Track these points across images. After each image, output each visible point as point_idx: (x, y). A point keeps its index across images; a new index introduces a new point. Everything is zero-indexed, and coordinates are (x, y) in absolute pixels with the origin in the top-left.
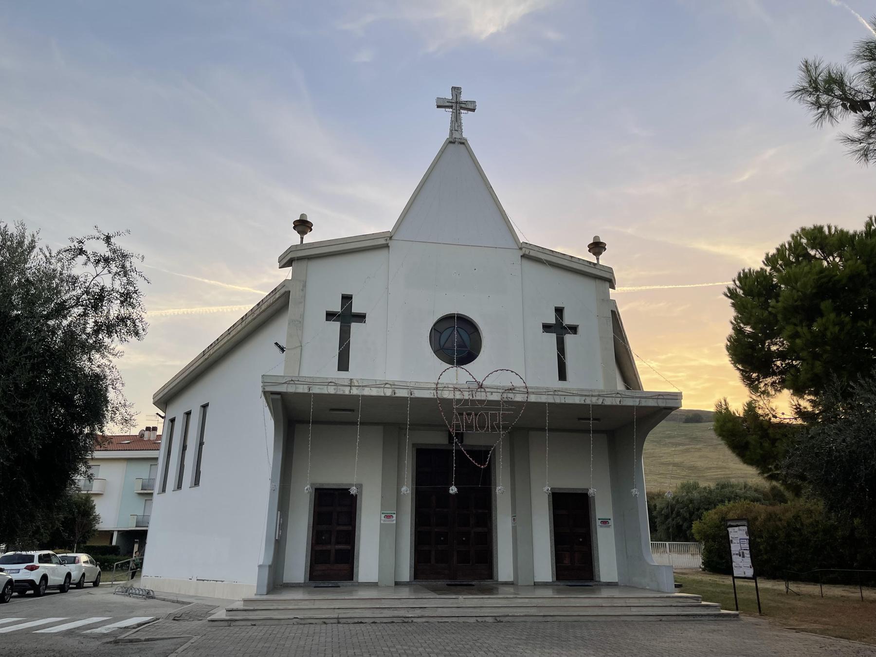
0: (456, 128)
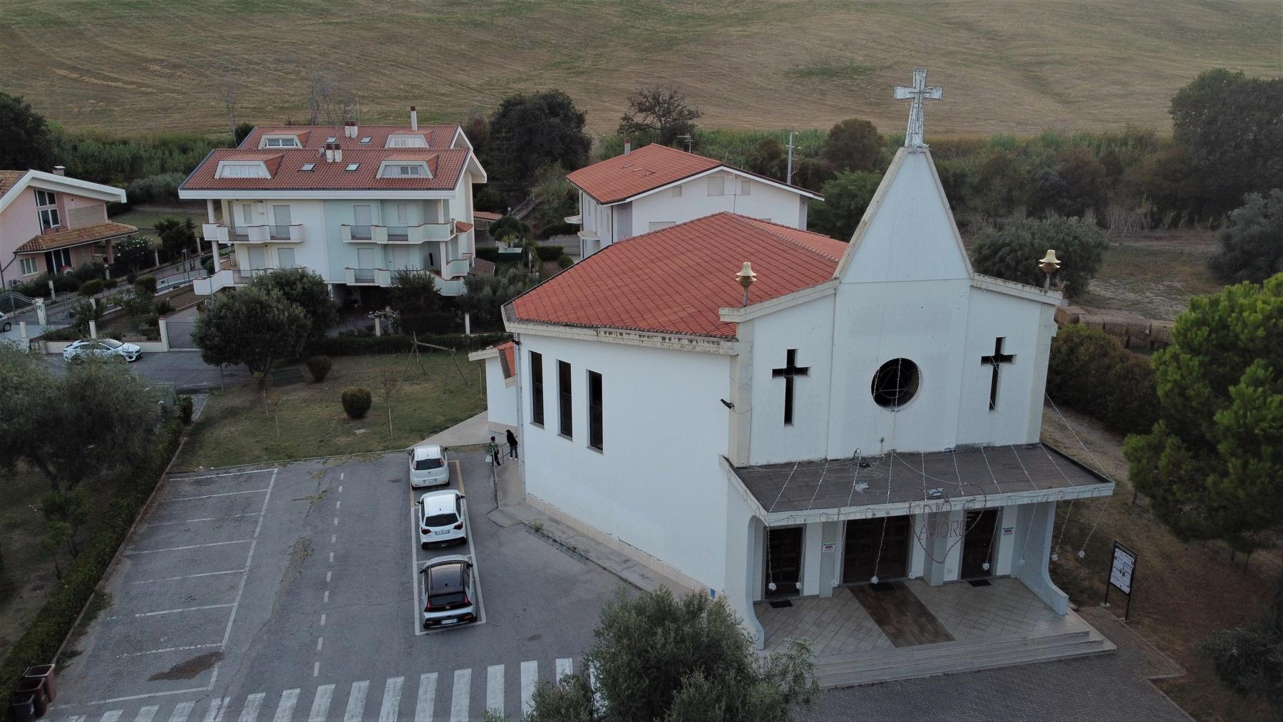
0: (917, 131)
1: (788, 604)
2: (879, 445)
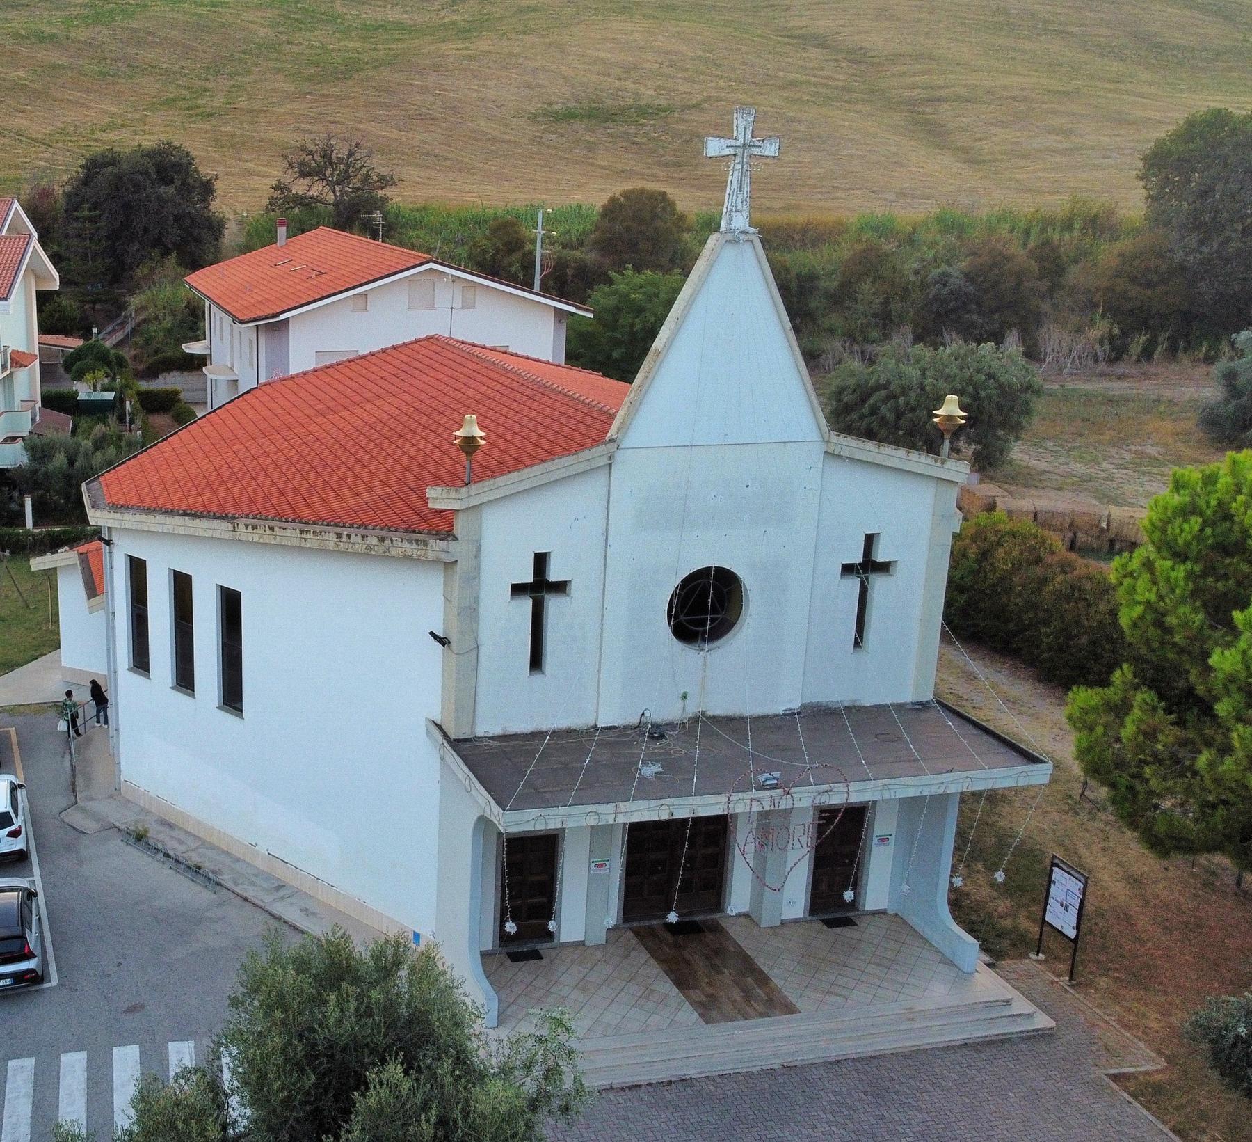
0: (739, 207)
1: (536, 955)
2: (680, 704)
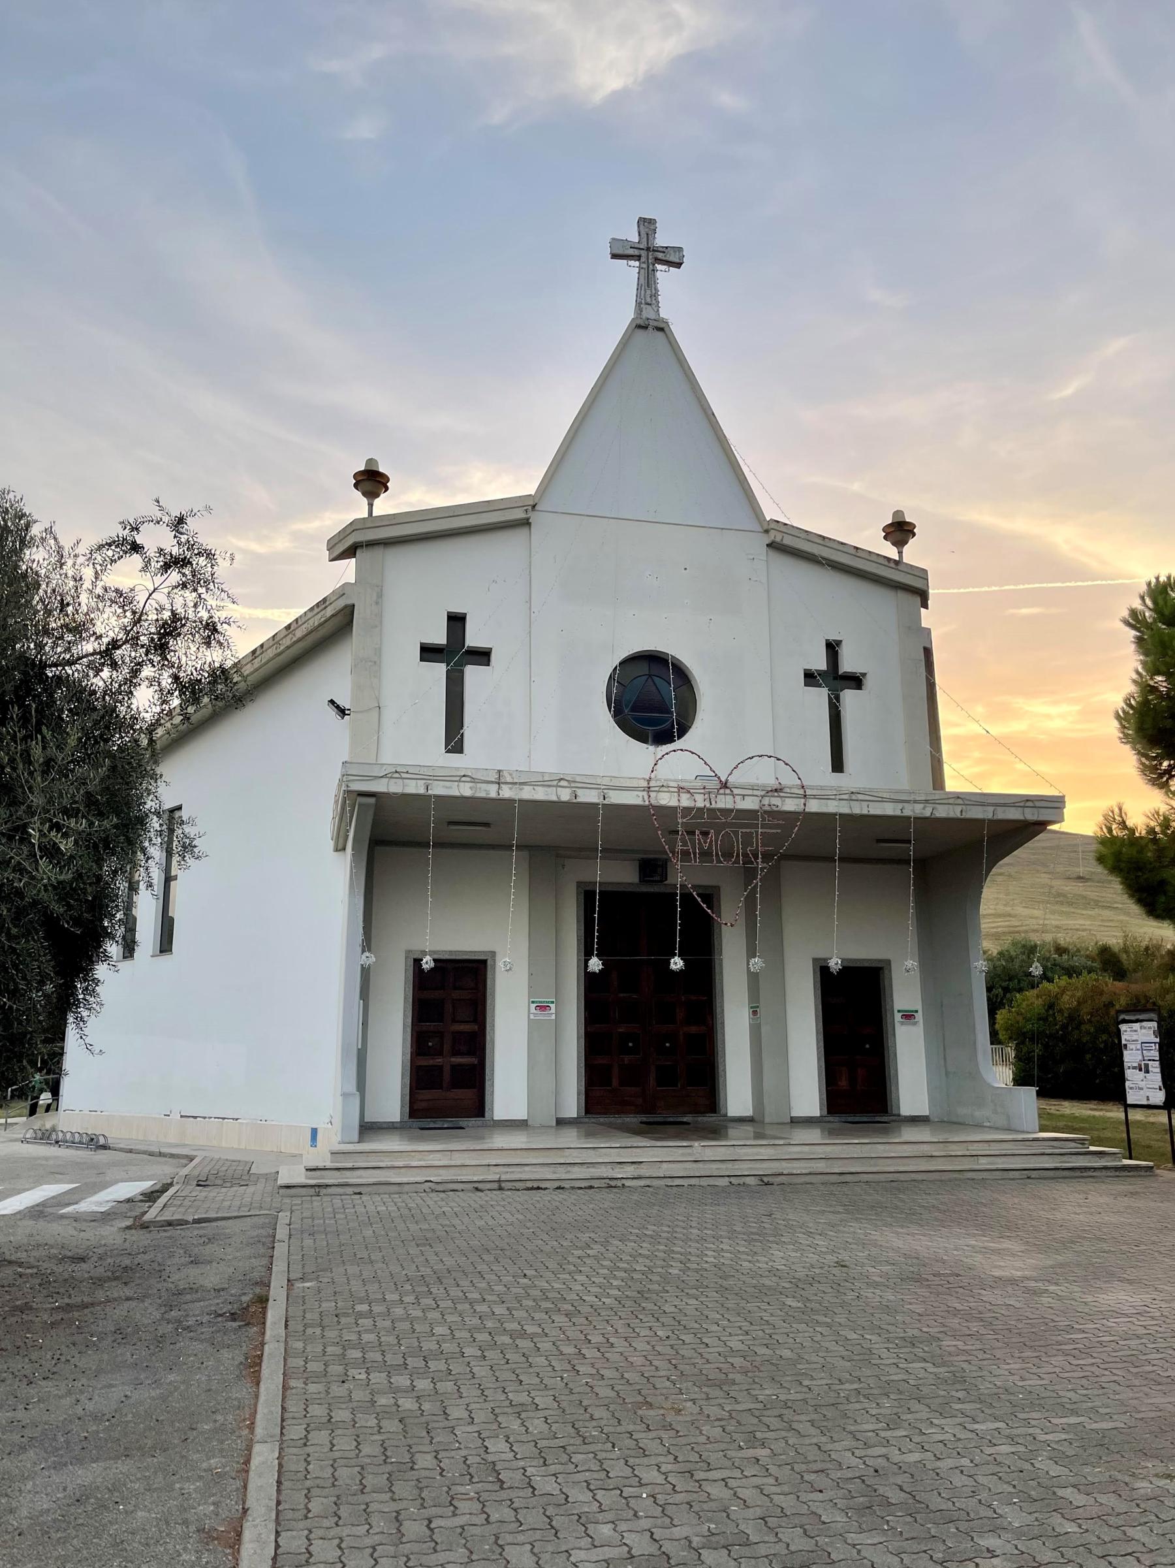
0: (648, 300)
